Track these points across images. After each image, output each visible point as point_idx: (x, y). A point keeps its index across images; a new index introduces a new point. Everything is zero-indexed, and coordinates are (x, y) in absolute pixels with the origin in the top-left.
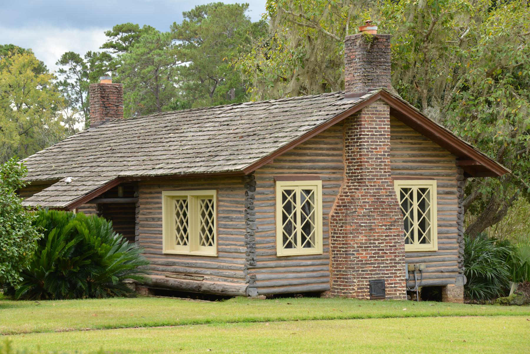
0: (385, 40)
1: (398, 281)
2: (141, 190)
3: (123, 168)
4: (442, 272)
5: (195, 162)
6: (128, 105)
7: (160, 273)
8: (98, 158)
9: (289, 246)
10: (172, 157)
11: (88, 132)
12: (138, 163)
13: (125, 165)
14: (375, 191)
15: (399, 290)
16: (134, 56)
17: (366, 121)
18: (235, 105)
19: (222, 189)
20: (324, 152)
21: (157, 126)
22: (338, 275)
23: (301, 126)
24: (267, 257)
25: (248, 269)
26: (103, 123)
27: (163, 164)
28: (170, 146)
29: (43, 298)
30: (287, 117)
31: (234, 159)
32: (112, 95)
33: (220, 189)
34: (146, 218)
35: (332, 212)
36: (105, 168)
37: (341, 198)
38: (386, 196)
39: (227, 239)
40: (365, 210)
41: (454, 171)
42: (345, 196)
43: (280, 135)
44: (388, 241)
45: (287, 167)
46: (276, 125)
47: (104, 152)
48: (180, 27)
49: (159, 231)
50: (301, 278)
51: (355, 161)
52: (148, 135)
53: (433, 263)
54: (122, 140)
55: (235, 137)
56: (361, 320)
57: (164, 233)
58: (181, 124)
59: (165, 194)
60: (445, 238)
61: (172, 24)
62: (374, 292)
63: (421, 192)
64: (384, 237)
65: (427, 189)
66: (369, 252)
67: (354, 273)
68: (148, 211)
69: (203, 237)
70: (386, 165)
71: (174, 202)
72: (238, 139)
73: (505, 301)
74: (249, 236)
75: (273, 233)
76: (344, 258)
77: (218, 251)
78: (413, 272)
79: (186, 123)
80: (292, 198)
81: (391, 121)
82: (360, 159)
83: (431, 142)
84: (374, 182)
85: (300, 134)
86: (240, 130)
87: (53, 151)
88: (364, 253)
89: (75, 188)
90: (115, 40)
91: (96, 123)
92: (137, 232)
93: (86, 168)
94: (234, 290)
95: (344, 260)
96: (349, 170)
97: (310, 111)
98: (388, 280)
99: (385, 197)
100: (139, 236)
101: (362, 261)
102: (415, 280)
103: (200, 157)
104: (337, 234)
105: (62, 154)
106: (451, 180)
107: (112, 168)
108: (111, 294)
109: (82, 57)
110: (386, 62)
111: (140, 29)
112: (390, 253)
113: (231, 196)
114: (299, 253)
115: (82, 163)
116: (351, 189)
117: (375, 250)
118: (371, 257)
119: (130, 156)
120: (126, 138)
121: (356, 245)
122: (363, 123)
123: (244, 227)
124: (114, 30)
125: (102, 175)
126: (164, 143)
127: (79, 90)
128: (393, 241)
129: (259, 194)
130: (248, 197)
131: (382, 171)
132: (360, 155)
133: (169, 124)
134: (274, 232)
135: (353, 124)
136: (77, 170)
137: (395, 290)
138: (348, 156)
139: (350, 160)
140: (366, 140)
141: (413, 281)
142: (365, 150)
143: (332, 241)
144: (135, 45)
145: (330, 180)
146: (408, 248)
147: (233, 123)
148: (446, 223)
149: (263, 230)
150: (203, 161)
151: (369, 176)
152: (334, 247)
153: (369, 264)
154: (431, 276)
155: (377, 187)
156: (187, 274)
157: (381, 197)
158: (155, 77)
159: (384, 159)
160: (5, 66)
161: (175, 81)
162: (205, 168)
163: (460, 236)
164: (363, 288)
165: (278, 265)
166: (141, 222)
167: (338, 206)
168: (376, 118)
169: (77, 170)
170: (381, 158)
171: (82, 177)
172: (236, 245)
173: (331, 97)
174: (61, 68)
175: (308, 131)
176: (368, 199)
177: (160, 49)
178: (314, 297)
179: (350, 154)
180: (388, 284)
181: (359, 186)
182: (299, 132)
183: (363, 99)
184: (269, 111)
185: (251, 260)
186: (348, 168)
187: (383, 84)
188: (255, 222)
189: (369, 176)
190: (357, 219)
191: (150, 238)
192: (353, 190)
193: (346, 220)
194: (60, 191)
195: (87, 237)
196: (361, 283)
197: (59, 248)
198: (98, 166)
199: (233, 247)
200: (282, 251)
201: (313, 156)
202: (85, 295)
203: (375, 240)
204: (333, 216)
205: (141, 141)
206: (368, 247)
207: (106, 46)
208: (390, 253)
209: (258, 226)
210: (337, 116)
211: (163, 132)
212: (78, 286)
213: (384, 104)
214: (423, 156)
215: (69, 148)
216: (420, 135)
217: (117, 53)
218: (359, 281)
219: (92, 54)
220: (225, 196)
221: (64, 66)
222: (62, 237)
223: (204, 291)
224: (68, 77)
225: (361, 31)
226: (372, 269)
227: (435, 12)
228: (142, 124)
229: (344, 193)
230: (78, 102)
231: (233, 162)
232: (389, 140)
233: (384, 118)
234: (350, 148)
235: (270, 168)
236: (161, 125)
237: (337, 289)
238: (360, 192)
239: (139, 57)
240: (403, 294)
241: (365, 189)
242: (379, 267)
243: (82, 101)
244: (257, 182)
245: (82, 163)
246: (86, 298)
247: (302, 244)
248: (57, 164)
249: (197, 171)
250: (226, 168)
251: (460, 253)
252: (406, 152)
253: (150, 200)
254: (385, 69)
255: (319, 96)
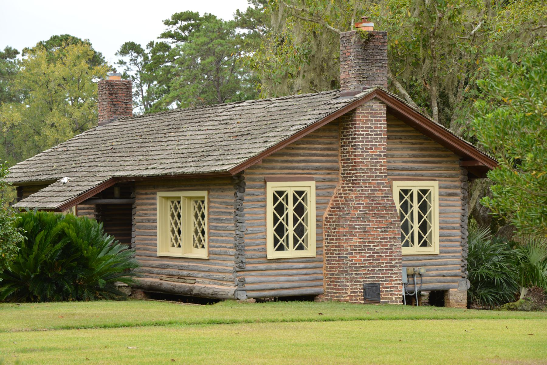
0: (381, 37)
1: (394, 285)
2: (137, 191)
3: (119, 168)
4: (444, 276)
5: (186, 162)
6: (187, 99)
7: (154, 276)
8: (98, 158)
9: (281, 248)
10: (167, 156)
11: (95, 130)
12: (134, 163)
13: (121, 165)
14: (370, 192)
15: (395, 294)
16: (194, 46)
17: (360, 120)
18: (238, 103)
19: (213, 190)
20: (318, 152)
21: (161, 125)
22: (331, 278)
23: (293, 125)
24: (257, 260)
25: (237, 272)
26: (111, 121)
27: (157, 164)
28: (167, 145)
29: (28, 301)
30: (282, 116)
31: (223, 160)
32: (120, 92)
33: (212, 190)
34: (142, 220)
35: (326, 214)
36: (102, 168)
37: (336, 199)
38: (382, 197)
39: (217, 241)
40: (359, 212)
41: (458, 172)
42: (340, 197)
43: (271, 134)
44: (384, 244)
45: (279, 167)
46: (270, 124)
47: (105, 152)
48: (244, 14)
49: (154, 232)
50: (293, 281)
51: (349, 161)
52: (150, 134)
53: (435, 267)
54: (125, 139)
55: (230, 137)
56: (332, 322)
57: (158, 234)
58: (183, 122)
59: (160, 194)
60: (448, 241)
61: (235, 12)
62: (369, 296)
63: (421, 194)
64: (380, 240)
65: (429, 190)
66: (363, 254)
67: (347, 277)
68: (144, 212)
69: (196, 239)
70: (381, 166)
71: (169, 203)
72: (231, 138)
73: (513, 307)
74: (238, 238)
75: (264, 235)
76: (337, 261)
77: (209, 253)
78: (413, 276)
79: (188, 121)
80: (409, 198)
81: (387, 120)
82: (355, 159)
83: (433, 141)
84: (369, 183)
85: (289, 134)
86: (237, 129)
87: (58, 150)
88: (358, 256)
89: (70, 189)
90: (173, 29)
91: (104, 122)
92: (133, 234)
93: (85, 168)
94: (223, 293)
95: (337, 263)
96: (345, 170)
97: (305, 110)
98: (383, 284)
99: (380, 199)
100: (135, 238)
101: (356, 264)
102: (414, 284)
103: (193, 157)
104: (330, 236)
105: (65, 153)
106: (454, 181)
107: (109, 168)
108: (99, 297)
109: (143, 47)
110: (382, 60)
111: (200, 17)
112: (386, 256)
113: (221, 197)
114: (290, 255)
115: (82, 163)
116: (345, 190)
117: (370, 253)
118: (365, 260)
119: (128, 155)
120: (129, 137)
121: (349, 248)
122: (357, 122)
123: (233, 229)
124: (173, 19)
125: (98, 176)
126: (163, 143)
127: (139, 83)
128: (389, 244)
129: (248, 195)
130: (237, 198)
131: (378, 171)
132: (355, 156)
133: (172, 123)
134: (264, 234)
135: (348, 123)
136: (75, 170)
137: (391, 295)
138: (344, 156)
139: (345, 160)
140: (361, 139)
141: (413, 285)
142: (360, 150)
143: (325, 243)
144: (195, 35)
145: (324, 180)
146: (406, 251)
147: (232, 122)
148: (448, 225)
149: (253, 232)
150: (195, 161)
151: (363, 176)
152: (328, 250)
153: (363, 267)
154: (432, 281)
155: (372, 188)
156: (180, 277)
157: (376, 199)
158: (215, 69)
159: (380, 159)
160: (59, 58)
161: (240, 73)
162: (194, 168)
163: (463, 239)
164: (357, 292)
165: (269, 268)
166: (138, 224)
167: (332, 208)
168: (372, 117)
169: (75, 170)
170: (376, 159)
171: (79, 177)
172: (226, 247)
173: (328, 95)
174: (121, 60)
175: (298, 131)
176: (363, 200)
177: (222, 39)
178: (305, 300)
179: (345, 155)
180: (384, 288)
181: (353, 187)
182: (290, 132)
183: (357, 97)
184: (268, 109)
185: (240, 263)
186: (343, 169)
187: (379, 82)
188: (244, 224)
189: (363, 176)
190: (350, 221)
191: (146, 239)
192: (347, 192)
193: (339, 222)
194: (55, 191)
195: (74, 240)
196: (354, 287)
197: (46, 251)
198: (96, 166)
199: (223, 249)
200: (272, 253)
201: (307, 156)
202: (72, 297)
203: (369, 242)
204: (327, 218)
205: (142, 140)
206: (362, 250)
207: (164, 36)
208: (386, 256)
209: (247, 228)
210: (330, 116)
211: (165, 131)
212: (64, 289)
213: (380, 103)
214: (424, 156)
215: (73, 146)
216: (421, 134)
217: (176, 44)
218: (352, 285)
219: (155, 43)
220: (215, 197)
221: (124, 57)
222: (49, 239)
223: (196, 294)
224: (128, 69)
225: (357, 28)
226: (367, 272)
227: (441, 7)
228: (147, 123)
229: (339, 194)
230: (139, 96)
231: (221, 163)
232: (385, 140)
233: (381, 117)
234: (345, 148)
235: (260, 169)
236: (164, 124)
237: (330, 293)
238: (354, 194)
239: (198, 47)
240: (399, 298)
241: (359, 191)
242: (374, 270)
243: (142, 95)
244: (246, 183)
245: (82, 163)
246: (73, 301)
247: (294, 247)
248: (59, 164)
249: (186, 171)
250: (213, 169)
251: (463, 257)
252: (406, 153)
253: (146, 201)
254: (382, 67)
255: (317, 95)
